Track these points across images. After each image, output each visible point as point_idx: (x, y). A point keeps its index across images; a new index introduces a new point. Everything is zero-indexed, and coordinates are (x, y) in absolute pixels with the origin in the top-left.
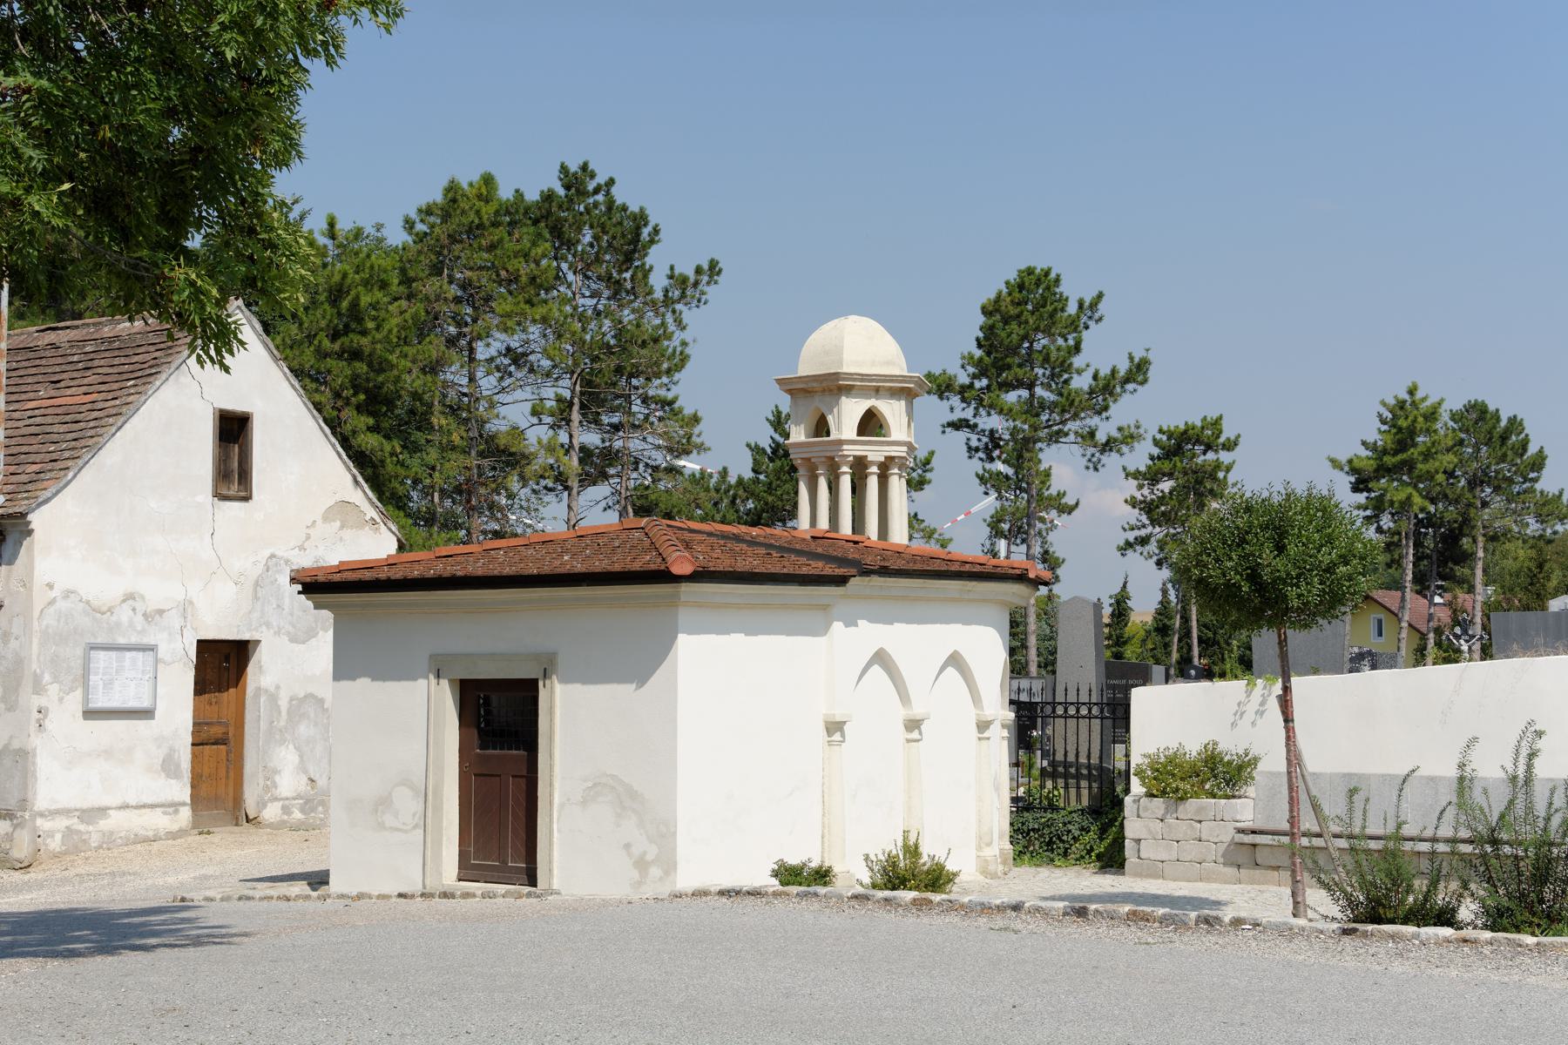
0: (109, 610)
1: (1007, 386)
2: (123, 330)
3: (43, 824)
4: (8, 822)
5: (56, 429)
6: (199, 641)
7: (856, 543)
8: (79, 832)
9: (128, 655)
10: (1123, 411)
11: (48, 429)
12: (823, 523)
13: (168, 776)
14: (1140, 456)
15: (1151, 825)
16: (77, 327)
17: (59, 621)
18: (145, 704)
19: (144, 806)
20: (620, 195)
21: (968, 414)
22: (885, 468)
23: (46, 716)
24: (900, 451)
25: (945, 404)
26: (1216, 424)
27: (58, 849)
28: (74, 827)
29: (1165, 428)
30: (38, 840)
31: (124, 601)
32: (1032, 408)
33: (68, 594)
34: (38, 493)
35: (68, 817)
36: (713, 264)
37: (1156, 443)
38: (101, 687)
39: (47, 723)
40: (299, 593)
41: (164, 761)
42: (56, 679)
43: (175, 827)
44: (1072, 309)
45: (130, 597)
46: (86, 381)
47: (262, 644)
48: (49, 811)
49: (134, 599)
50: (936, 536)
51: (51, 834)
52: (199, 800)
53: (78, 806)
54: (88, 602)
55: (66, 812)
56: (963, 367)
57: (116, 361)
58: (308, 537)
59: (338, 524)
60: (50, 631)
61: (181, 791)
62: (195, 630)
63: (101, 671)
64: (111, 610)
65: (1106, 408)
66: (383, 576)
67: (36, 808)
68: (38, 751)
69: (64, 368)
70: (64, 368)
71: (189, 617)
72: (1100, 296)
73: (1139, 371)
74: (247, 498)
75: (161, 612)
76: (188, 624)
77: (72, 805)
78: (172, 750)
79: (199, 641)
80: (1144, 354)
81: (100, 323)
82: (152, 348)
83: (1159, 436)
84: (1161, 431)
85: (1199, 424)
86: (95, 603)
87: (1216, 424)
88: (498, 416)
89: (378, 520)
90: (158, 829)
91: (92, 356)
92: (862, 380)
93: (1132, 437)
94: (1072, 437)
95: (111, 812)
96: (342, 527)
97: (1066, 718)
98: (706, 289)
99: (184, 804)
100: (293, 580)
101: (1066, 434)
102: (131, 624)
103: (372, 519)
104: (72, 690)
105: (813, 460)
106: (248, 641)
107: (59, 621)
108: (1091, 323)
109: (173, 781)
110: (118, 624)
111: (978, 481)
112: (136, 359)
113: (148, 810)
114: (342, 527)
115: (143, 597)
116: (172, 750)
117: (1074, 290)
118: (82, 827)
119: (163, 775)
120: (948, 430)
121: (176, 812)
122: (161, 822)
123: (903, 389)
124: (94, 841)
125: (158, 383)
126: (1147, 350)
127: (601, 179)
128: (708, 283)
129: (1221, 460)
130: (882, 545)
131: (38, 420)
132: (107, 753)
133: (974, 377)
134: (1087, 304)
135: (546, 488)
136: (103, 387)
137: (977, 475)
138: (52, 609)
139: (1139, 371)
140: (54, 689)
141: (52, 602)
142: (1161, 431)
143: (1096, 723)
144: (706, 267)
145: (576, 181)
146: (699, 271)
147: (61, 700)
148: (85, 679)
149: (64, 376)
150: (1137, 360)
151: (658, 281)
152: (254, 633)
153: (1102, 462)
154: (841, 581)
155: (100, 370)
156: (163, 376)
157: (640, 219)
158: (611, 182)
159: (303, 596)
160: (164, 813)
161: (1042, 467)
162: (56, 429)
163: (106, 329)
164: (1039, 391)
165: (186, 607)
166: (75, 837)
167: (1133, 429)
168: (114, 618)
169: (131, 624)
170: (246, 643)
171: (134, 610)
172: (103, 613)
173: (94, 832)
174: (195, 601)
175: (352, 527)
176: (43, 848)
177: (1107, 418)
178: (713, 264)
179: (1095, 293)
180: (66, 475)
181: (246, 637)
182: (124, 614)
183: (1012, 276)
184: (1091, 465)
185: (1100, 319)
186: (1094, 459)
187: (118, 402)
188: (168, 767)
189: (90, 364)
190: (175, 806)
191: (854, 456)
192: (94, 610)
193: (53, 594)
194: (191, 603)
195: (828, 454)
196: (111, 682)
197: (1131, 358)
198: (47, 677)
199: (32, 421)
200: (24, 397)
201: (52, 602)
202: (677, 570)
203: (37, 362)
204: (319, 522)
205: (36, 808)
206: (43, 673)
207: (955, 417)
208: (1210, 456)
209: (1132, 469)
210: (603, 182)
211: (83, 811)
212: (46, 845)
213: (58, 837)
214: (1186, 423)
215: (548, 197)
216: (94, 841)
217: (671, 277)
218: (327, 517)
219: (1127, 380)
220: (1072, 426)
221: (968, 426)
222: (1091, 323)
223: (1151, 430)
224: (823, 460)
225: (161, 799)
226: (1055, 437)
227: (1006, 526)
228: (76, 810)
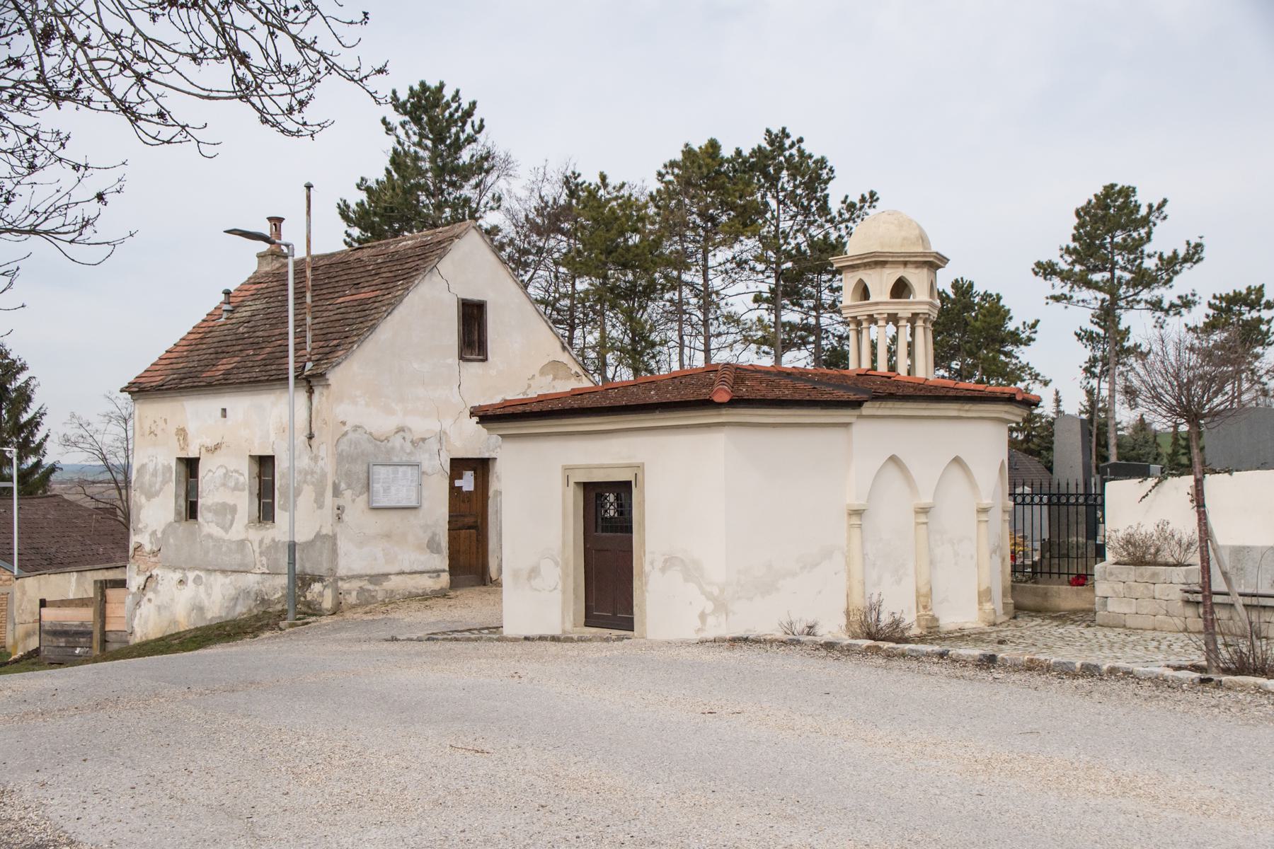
0: (386, 439)
1: (1096, 269)
2: (401, 247)
3: (344, 586)
4: (320, 584)
5: (351, 316)
6: (451, 459)
7: (889, 378)
8: (369, 591)
9: (401, 469)
10: (1185, 282)
11: (347, 316)
12: (866, 364)
13: (432, 552)
14: (1199, 315)
15: (1115, 586)
16: (374, 247)
17: (350, 447)
18: (414, 504)
19: (415, 573)
20: (807, 147)
21: (1066, 290)
22: (913, 319)
23: (343, 512)
24: (923, 309)
25: (1049, 283)
26: (1260, 290)
27: (354, 602)
28: (365, 587)
29: (1218, 296)
30: (340, 596)
31: (397, 432)
32: (1111, 287)
33: (356, 428)
34: (334, 360)
35: (361, 580)
36: (872, 194)
37: (1210, 305)
38: (382, 491)
39: (344, 517)
40: (477, 423)
41: (429, 541)
42: (349, 486)
43: (437, 587)
44: (1143, 211)
45: (401, 430)
46: (374, 283)
47: (498, 461)
48: (347, 577)
49: (404, 431)
50: (1040, 378)
51: (349, 592)
52: (454, 569)
53: (368, 572)
54: (371, 434)
55: (360, 577)
56: (1062, 256)
57: (394, 269)
58: (529, 386)
59: (551, 376)
60: (344, 454)
61: (442, 562)
62: (449, 451)
63: (381, 481)
64: (387, 439)
65: (1170, 280)
66: (536, 409)
67: (338, 575)
68: (338, 536)
69: (364, 274)
70: (364, 274)
71: (444, 443)
72: (1165, 201)
73: (1194, 254)
74: (485, 360)
75: (424, 440)
76: (444, 448)
77: (363, 572)
78: (434, 535)
79: (451, 459)
80: (1198, 241)
81: (388, 243)
82: (417, 258)
83: (1213, 301)
84: (1215, 297)
85: (1244, 292)
86: (375, 434)
87: (1260, 290)
88: (727, 304)
89: (581, 373)
90: (425, 589)
91: (382, 265)
92: (892, 257)
93: (1189, 302)
94: (1143, 305)
95: (392, 577)
96: (554, 379)
97: (1023, 505)
98: (868, 211)
99: (444, 571)
100: (472, 414)
101: (1139, 302)
102: (402, 448)
103: (576, 372)
104: (361, 494)
105: (858, 318)
106: (489, 459)
107: (350, 447)
108: (1158, 222)
109: (435, 555)
110: (393, 448)
111: (1077, 338)
112: (407, 266)
113: (418, 575)
114: (554, 379)
115: (410, 430)
116: (434, 535)
117: (1144, 198)
118: (371, 587)
119: (428, 551)
120: (1050, 301)
121: (438, 576)
122: (428, 583)
123: (925, 262)
124: (380, 596)
125: (416, 282)
126: (1201, 237)
127: (794, 138)
128: (869, 207)
129: (1263, 317)
130: (910, 379)
131: (342, 310)
132: (388, 536)
133: (1073, 263)
134: (1155, 208)
135: (764, 352)
136: (384, 286)
137: (1076, 334)
138: (345, 439)
139: (1194, 254)
140: (348, 494)
141: (346, 434)
142: (1215, 297)
143: (1045, 508)
144: (867, 196)
145: (777, 140)
146: (863, 199)
147: (353, 501)
148: (368, 486)
149: (363, 280)
150: (1193, 244)
151: (835, 205)
152: (492, 453)
153: (1166, 322)
154: (858, 404)
155: (384, 275)
156: (421, 277)
157: (822, 162)
158: (801, 140)
159: (480, 425)
160: (430, 577)
161: (1122, 327)
162: (351, 316)
163: (392, 247)
164: (1118, 273)
165: (441, 437)
166: (366, 594)
167: (1190, 297)
168: (390, 445)
169: (402, 448)
170: (488, 460)
171: (404, 438)
172: (382, 441)
173: (379, 591)
174: (448, 431)
175: (562, 379)
176: (343, 602)
177: (1171, 287)
178: (872, 194)
179: (1161, 200)
180: (352, 347)
181: (486, 456)
182: (397, 441)
183: (1099, 190)
184: (1158, 325)
185: (1165, 218)
186: (1160, 321)
187: (390, 296)
188: (432, 546)
189: (378, 271)
190: (438, 572)
191: (888, 314)
192: (373, 438)
193: (346, 428)
194: (445, 433)
195: (868, 313)
196: (389, 488)
197: (1188, 243)
198: (343, 486)
199: (339, 311)
200: (337, 295)
201: (346, 434)
202: (717, 399)
203: (349, 271)
204: (537, 375)
205: (338, 575)
206: (340, 482)
207: (1057, 292)
208: (1255, 314)
209: (1191, 325)
210: (795, 140)
211: (371, 576)
212: (345, 599)
213: (354, 594)
214: (1234, 291)
215: (759, 151)
216: (380, 596)
217: (844, 202)
218: (543, 372)
219: (1185, 260)
220: (1145, 295)
221: (1066, 298)
222: (1158, 222)
223: (1205, 297)
224: (866, 317)
225: (428, 568)
226: (1131, 305)
227: (1097, 370)
228: (367, 576)
